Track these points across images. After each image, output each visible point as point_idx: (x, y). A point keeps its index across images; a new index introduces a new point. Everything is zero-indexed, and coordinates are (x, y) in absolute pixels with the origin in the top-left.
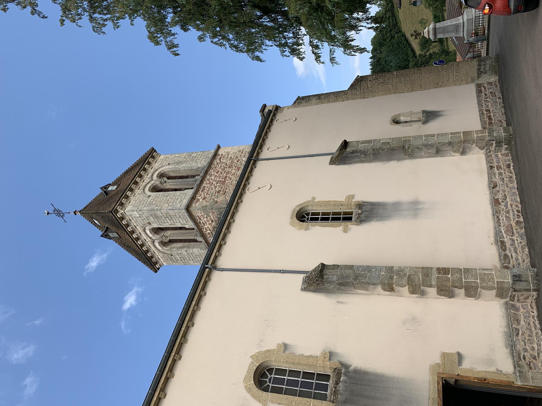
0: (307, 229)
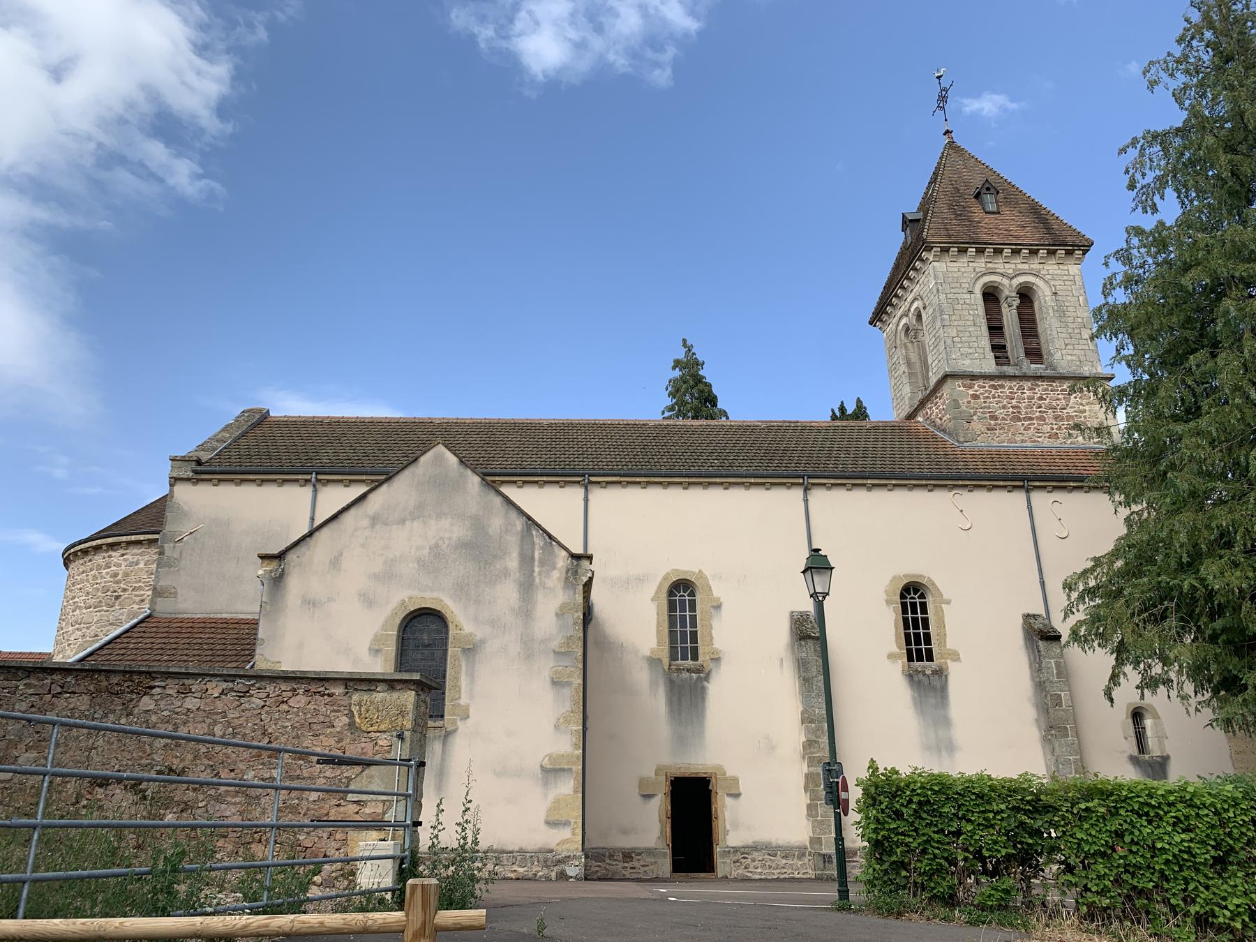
0: (888, 602)
